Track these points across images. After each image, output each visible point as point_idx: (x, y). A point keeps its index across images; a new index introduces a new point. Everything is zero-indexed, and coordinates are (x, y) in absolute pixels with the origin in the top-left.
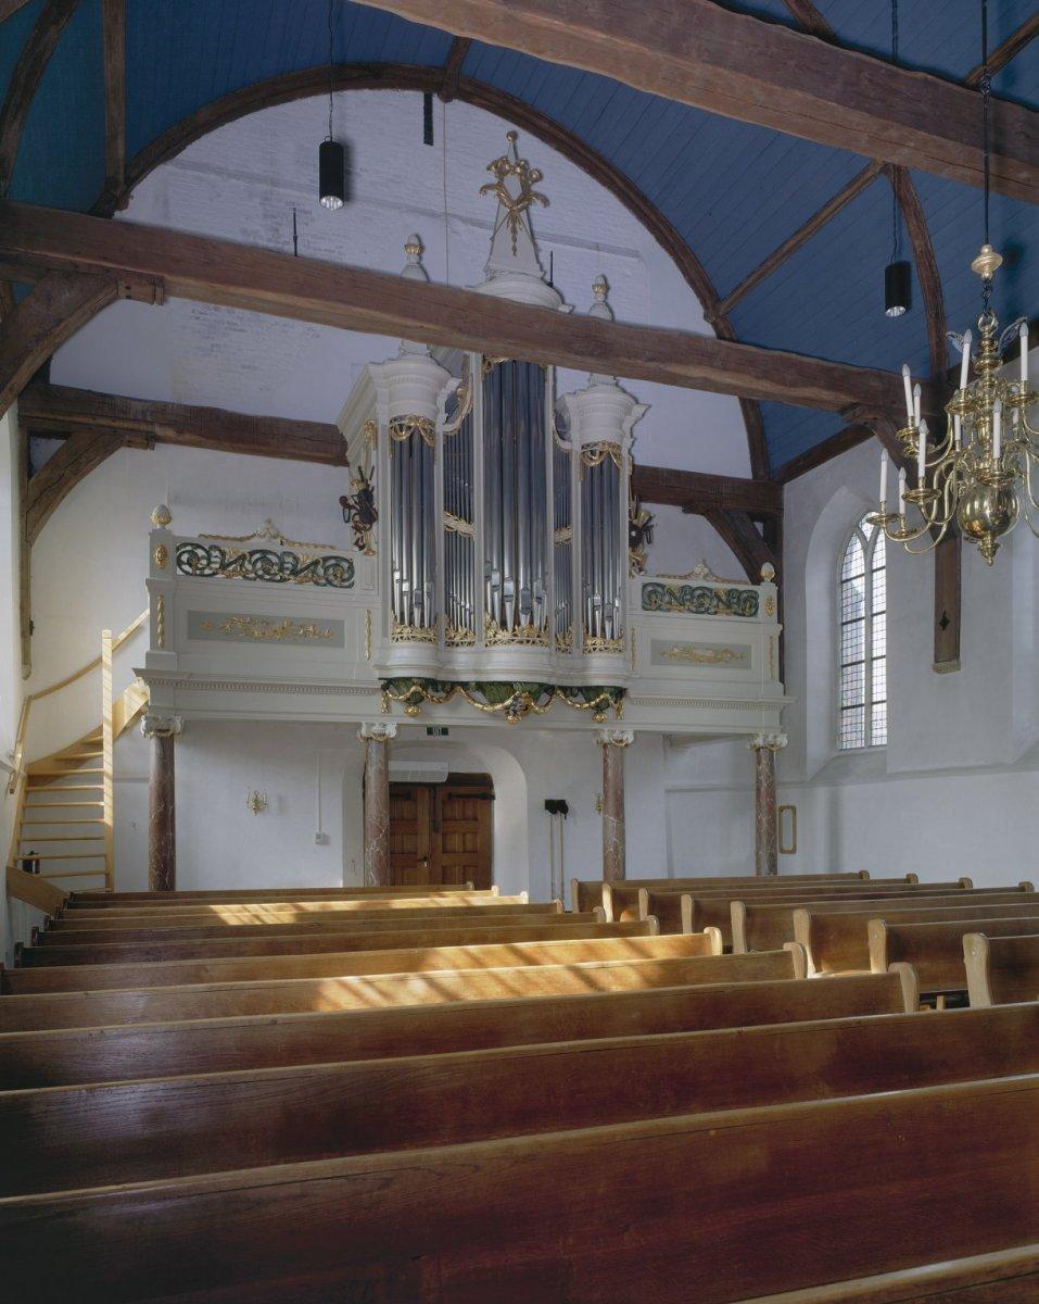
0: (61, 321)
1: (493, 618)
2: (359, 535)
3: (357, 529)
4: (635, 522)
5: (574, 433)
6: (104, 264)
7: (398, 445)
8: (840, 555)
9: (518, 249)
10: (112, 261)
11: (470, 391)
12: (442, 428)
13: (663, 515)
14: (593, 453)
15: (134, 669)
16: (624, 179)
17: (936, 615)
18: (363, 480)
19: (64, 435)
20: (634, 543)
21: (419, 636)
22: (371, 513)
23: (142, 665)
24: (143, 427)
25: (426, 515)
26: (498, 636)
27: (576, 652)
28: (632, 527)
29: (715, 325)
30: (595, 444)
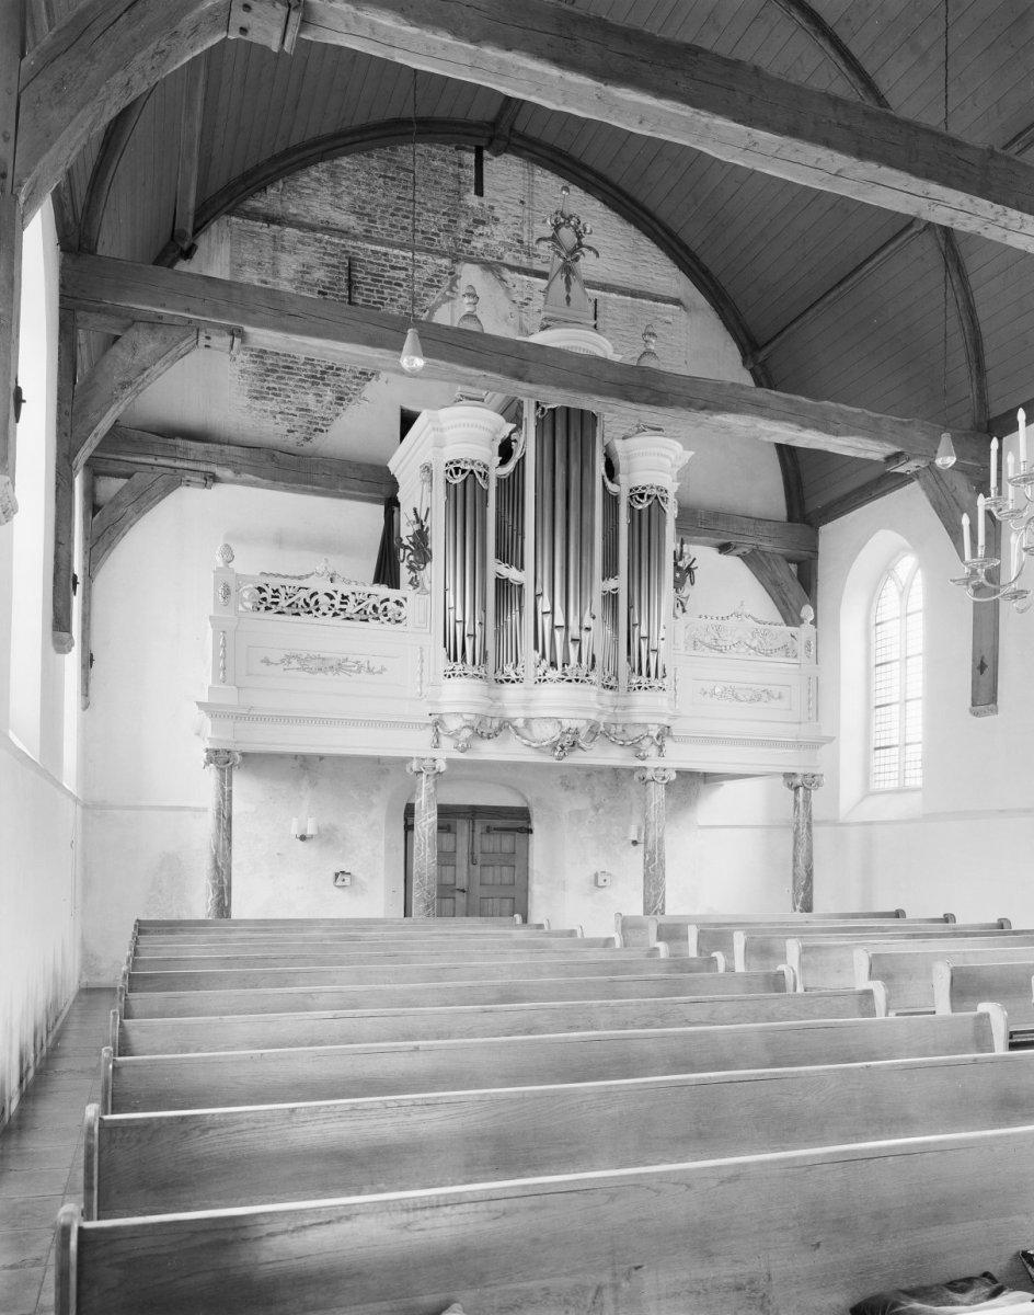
0: (145, 369)
1: (543, 656)
2: (413, 574)
4: (680, 564)
5: (621, 477)
6: (187, 315)
7: (452, 487)
8: (874, 595)
9: (572, 300)
10: (195, 314)
11: (523, 435)
12: (498, 471)
13: (703, 555)
15: (197, 703)
16: (668, 231)
17: (973, 660)
18: (418, 520)
19: (129, 476)
20: (678, 584)
22: (425, 553)
23: (205, 698)
24: (203, 467)
27: (622, 691)
28: (677, 568)
29: (752, 371)
30: (644, 488)
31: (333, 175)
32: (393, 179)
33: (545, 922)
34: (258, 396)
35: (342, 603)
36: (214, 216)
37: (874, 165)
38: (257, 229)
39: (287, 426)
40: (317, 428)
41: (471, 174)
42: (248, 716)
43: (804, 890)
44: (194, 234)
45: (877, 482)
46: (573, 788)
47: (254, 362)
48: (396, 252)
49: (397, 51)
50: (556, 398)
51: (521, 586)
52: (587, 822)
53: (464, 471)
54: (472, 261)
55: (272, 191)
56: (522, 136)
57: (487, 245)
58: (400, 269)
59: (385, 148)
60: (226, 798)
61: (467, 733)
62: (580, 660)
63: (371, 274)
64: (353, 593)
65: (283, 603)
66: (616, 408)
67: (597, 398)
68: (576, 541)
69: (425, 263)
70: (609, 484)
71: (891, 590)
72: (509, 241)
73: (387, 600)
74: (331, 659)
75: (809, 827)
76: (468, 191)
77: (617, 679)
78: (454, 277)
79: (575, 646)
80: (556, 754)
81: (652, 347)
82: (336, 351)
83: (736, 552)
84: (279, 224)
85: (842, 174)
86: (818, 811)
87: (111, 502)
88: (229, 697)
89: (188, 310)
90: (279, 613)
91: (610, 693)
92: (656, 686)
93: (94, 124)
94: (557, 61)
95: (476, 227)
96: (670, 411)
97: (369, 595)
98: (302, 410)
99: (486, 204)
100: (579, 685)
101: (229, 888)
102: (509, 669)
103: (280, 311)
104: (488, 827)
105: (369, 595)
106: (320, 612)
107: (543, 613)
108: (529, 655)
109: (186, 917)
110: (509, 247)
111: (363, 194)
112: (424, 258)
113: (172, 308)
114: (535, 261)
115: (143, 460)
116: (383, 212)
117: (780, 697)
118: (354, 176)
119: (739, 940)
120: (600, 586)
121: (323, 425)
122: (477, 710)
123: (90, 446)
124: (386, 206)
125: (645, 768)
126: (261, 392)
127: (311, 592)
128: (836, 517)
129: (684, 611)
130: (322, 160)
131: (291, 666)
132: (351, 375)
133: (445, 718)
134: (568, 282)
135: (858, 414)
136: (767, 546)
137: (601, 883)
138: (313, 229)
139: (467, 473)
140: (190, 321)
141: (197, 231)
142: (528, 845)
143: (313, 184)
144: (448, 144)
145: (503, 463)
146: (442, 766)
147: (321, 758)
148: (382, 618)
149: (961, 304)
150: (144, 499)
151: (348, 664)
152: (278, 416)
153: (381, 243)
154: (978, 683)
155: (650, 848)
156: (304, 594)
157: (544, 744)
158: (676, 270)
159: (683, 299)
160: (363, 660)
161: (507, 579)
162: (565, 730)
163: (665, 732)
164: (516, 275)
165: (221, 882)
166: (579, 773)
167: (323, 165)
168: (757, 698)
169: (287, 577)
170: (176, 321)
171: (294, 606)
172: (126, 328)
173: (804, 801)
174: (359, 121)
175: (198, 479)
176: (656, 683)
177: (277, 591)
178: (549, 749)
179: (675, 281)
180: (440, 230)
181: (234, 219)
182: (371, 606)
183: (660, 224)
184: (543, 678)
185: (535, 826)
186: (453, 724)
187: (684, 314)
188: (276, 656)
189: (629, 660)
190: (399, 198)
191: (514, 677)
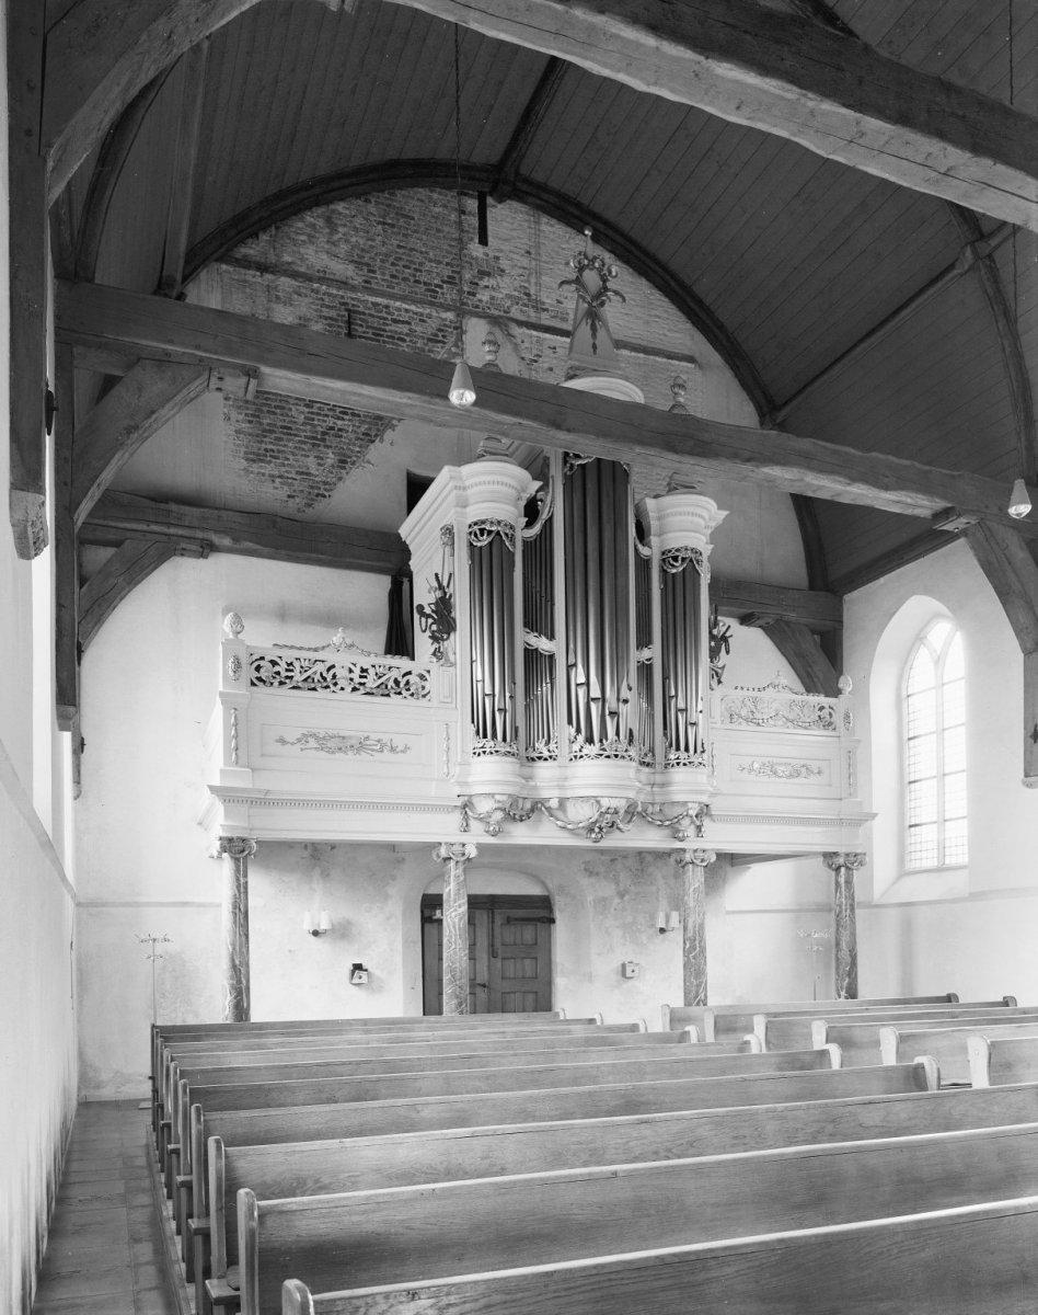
0: (153, 412)
1: (578, 731)
3: (434, 638)
4: (715, 632)
5: (654, 540)
7: (477, 551)
10: (206, 351)
11: (550, 494)
14: (675, 559)
17: (1025, 729)
18: (441, 587)
19: (117, 544)
20: (714, 653)
21: (503, 750)
23: (217, 782)
24: (200, 534)
25: (508, 636)
26: (585, 751)
27: (659, 768)
28: (712, 637)
30: (678, 550)
31: (328, 220)
32: (393, 226)
33: (596, 1016)
34: (256, 458)
35: (361, 677)
36: (204, 262)
37: (988, 162)
38: (250, 278)
39: (286, 490)
40: (319, 492)
41: (475, 221)
42: (261, 801)
43: (849, 975)
44: (183, 282)
45: (918, 540)
46: (597, 874)
47: (250, 422)
48: (398, 304)
49: (473, 14)
50: (591, 449)
51: (552, 657)
52: (612, 910)
53: (490, 532)
54: (478, 315)
55: (264, 237)
56: (527, 181)
57: (492, 298)
58: (403, 322)
59: (383, 191)
60: (241, 889)
61: (499, 815)
62: (618, 734)
63: (373, 328)
64: (373, 666)
65: (298, 677)
66: (655, 460)
67: (638, 449)
68: (596, 611)
69: (429, 316)
70: (640, 546)
71: (923, 659)
72: (516, 294)
73: (409, 673)
74: (350, 737)
75: (852, 909)
76: (472, 239)
77: (654, 755)
78: (460, 330)
79: (612, 719)
80: (593, 836)
81: (682, 400)
82: (360, 395)
83: (760, 622)
84: (272, 273)
85: (951, 173)
86: (859, 896)
87: (100, 572)
88: (242, 781)
89: (198, 347)
90: (294, 688)
91: (647, 770)
92: (696, 763)
93: (130, 83)
94: (655, 28)
95: (481, 279)
96: (714, 463)
97: (390, 668)
98: (302, 473)
99: (491, 254)
100: (620, 762)
101: (248, 988)
102: (540, 745)
103: (297, 350)
104: (508, 917)
105: (390, 668)
106: (339, 687)
107: (578, 685)
108: (563, 731)
109: (191, 1021)
110: (516, 301)
111: (361, 241)
112: (428, 311)
113: (183, 344)
114: (544, 315)
115: (134, 526)
116: (382, 261)
117: (819, 773)
118: (351, 222)
119: (759, 1024)
120: (636, 656)
121: (325, 490)
122: (510, 790)
123: (92, 497)
124: (386, 255)
125: (684, 850)
126: (258, 455)
127: (328, 665)
128: (863, 584)
129: (719, 682)
130: (318, 205)
131: (309, 746)
132: (353, 436)
133: (474, 800)
134: (594, 329)
135: (905, 466)
136: (792, 616)
137: (629, 974)
138: (309, 279)
139: (493, 535)
140: (201, 359)
141: (186, 278)
142: (550, 935)
143: (308, 230)
144: (450, 188)
145: (529, 525)
146: (472, 852)
147: (333, 846)
148: (404, 693)
149: (1008, 350)
150: (136, 570)
151: (368, 743)
152: (278, 480)
153: (382, 294)
154: (1031, 752)
155: (690, 934)
156: (320, 668)
157: (581, 825)
158: (689, 326)
159: (697, 356)
160: (385, 738)
161: (536, 649)
162: (603, 810)
163: (704, 810)
164: (525, 330)
165: (239, 982)
166: (603, 858)
167: (320, 210)
168: (796, 774)
169: (301, 648)
170: (185, 360)
171: (310, 680)
172: (130, 367)
173: (846, 882)
174: (354, 163)
175: (194, 547)
176: (696, 759)
177: (291, 664)
178: (584, 832)
179: (688, 338)
180: (443, 282)
181: (224, 267)
182: (392, 679)
183: (673, 276)
184: (579, 754)
185: (558, 915)
186: (484, 806)
187: (699, 373)
188: (291, 736)
189: (665, 735)
190: (399, 246)
191: (546, 754)
